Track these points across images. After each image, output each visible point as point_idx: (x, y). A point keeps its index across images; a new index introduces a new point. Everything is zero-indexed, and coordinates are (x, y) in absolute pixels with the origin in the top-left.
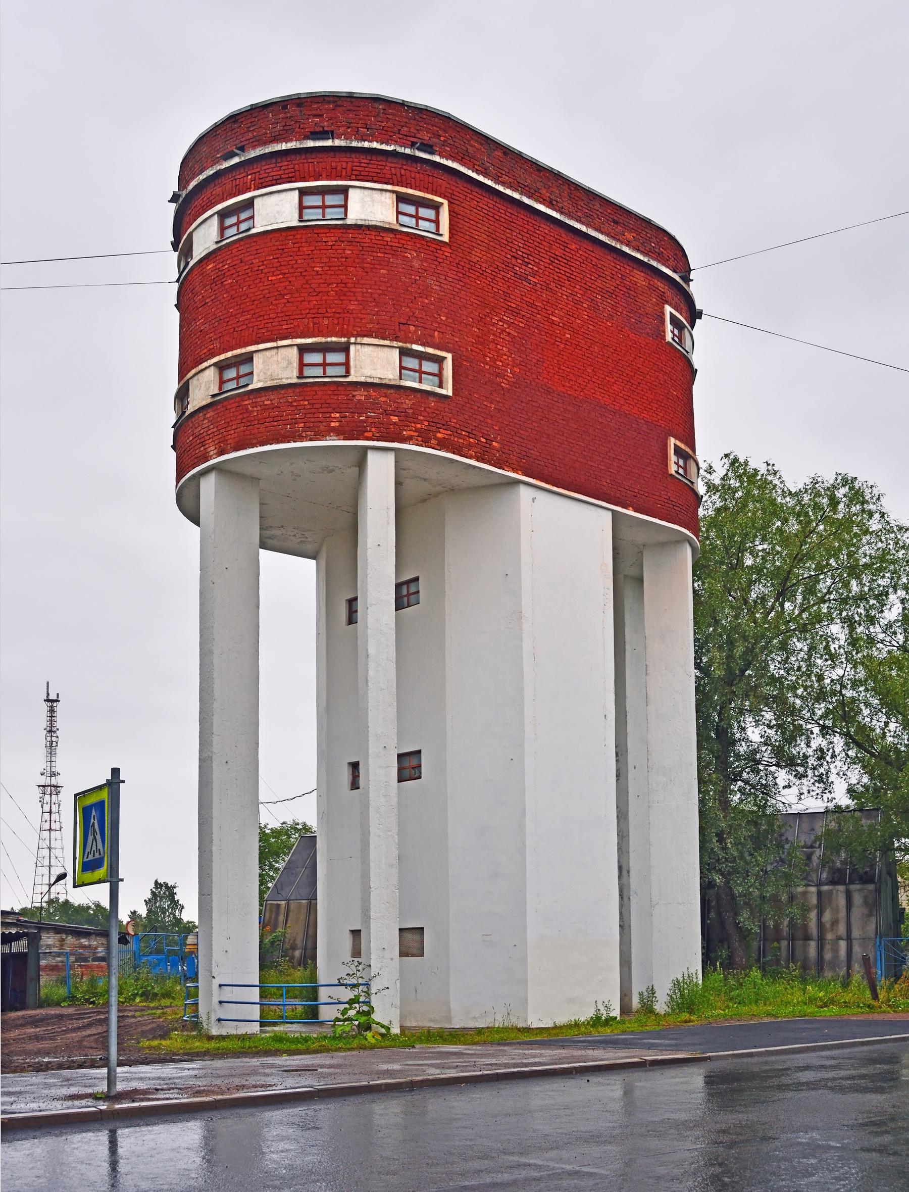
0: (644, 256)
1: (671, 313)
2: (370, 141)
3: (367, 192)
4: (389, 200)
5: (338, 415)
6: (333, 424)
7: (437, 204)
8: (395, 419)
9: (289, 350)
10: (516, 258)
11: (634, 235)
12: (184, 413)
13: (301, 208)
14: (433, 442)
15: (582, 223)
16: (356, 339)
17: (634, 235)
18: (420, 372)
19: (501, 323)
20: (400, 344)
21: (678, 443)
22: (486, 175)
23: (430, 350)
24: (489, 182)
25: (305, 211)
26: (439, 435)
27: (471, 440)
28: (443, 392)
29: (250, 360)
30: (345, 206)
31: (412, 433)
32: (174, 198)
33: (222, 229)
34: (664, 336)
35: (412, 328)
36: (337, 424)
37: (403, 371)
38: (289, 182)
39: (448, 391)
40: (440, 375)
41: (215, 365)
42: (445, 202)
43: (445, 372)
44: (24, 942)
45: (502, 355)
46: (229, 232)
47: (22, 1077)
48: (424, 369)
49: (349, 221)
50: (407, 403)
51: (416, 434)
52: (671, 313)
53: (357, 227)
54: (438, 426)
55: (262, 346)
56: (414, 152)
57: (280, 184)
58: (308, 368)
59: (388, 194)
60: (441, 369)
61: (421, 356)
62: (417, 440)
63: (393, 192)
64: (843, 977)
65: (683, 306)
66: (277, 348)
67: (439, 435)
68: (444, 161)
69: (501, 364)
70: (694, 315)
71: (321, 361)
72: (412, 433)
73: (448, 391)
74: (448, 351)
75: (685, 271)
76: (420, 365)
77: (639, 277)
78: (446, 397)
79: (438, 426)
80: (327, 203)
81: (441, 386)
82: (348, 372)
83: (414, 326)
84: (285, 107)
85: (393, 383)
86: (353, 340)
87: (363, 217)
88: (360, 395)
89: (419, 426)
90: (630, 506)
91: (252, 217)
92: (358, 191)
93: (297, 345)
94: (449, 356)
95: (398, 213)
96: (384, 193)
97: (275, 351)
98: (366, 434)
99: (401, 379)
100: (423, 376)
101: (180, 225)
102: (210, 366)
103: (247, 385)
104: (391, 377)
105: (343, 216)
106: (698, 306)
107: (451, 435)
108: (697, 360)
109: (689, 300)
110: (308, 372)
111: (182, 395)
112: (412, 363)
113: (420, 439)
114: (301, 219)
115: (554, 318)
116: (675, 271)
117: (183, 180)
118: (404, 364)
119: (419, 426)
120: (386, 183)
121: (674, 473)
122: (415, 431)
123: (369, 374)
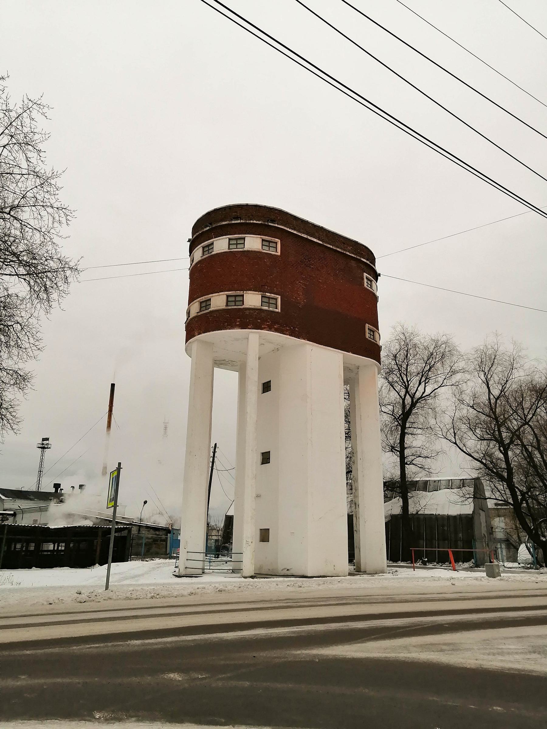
0: (355, 255)
1: (366, 276)
4: (260, 241)
5: (239, 320)
6: (237, 323)
8: (259, 321)
9: (223, 296)
10: (306, 259)
12: (189, 317)
13: (229, 244)
15: (330, 245)
18: (269, 303)
22: (295, 229)
24: (295, 232)
25: (229, 302)
26: (275, 327)
27: (288, 328)
28: (277, 310)
29: (210, 300)
30: (244, 243)
31: (265, 326)
32: (189, 240)
33: (203, 252)
34: (364, 285)
36: (239, 323)
37: (263, 246)
38: (225, 235)
39: (279, 310)
40: (276, 304)
41: (198, 301)
42: (279, 241)
43: (278, 303)
44: (126, 531)
45: (300, 295)
46: (206, 253)
48: (271, 302)
49: (245, 249)
50: (263, 315)
51: (267, 326)
52: (366, 276)
53: (248, 251)
54: (275, 323)
57: (222, 236)
58: (232, 245)
59: (259, 239)
60: (276, 302)
61: (269, 298)
63: (261, 238)
65: (372, 273)
66: (219, 295)
67: (275, 327)
68: (279, 226)
70: (376, 276)
71: (236, 243)
72: (265, 326)
73: (279, 310)
75: (372, 258)
76: (269, 301)
77: (353, 264)
78: (278, 312)
79: (275, 323)
80: (236, 300)
81: (276, 308)
82: (243, 304)
84: (225, 209)
86: (245, 292)
88: (247, 312)
89: (268, 323)
92: (248, 238)
94: (279, 297)
95: (262, 245)
97: (218, 296)
98: (249, 327)
99: (262, 306)
100: (270, 248)
101: (191, 251)
102: (195, 341)
103: (211, 253)
104: (258, 305)
105: (243, 247)
106: (378, 272)
107: (279, 326)
108: (378, 294)
109: (374, 271)
110: (231, 247)
111: (188, 313)
112: (265, 300)
113: (268, 328)
114: (229, 248)
116: (367, 260)
117: (193, 233)
118: (263, 300)
119: (268, 323)
120: (259, 235)
121: (368, 337)
123: (250, 304)
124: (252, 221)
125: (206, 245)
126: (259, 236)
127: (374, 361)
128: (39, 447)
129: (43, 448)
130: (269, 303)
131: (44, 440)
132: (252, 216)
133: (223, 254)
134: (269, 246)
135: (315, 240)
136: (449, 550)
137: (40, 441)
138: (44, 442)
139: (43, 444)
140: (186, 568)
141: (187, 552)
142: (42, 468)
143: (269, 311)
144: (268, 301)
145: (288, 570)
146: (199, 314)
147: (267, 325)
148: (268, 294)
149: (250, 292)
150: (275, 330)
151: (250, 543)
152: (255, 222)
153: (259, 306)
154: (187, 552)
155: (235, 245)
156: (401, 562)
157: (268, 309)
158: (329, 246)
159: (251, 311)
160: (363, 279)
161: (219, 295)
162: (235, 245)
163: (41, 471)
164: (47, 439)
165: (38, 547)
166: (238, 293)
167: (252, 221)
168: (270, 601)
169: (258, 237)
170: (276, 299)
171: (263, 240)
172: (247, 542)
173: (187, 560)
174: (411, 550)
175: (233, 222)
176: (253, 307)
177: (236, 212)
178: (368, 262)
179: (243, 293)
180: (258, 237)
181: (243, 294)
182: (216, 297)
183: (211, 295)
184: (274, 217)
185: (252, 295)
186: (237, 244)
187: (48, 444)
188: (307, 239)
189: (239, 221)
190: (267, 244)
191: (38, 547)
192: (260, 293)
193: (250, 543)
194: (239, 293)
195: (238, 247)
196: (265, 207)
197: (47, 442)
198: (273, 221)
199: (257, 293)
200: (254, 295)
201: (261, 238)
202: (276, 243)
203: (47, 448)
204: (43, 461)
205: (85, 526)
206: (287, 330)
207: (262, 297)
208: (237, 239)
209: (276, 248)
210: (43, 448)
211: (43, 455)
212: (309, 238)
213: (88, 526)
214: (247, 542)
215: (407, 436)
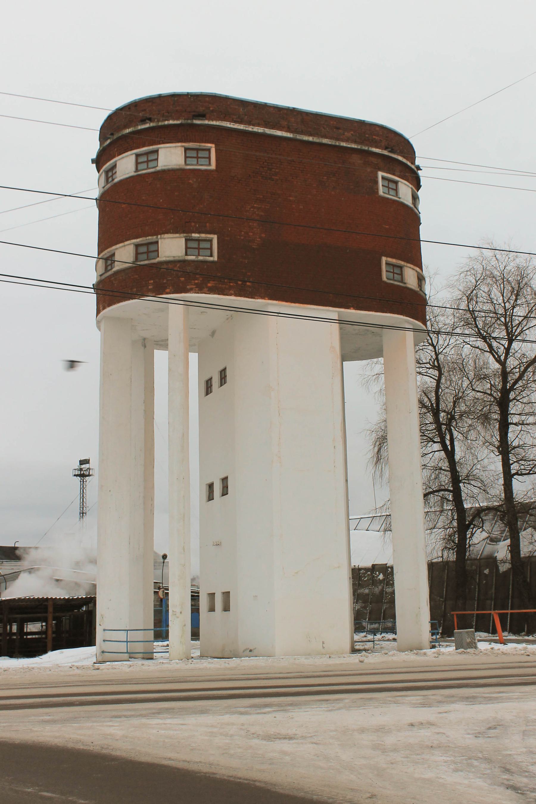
2: (168, 120)
3: (168, 149)
5: (152, 281)
7: (209, 148)
8: (183, 279)
11: (352, 133)
14: (206, 290)
16: (161, 236)
17: (352, 133)
19: (252, 209)
20: (185, 235)
21: (390, 260)
22: (241, 122)
23: (203, 235)
24: (241, 127)
34: (378, 192)
35: (193, 224)
39: (215, 258)
40: (211, 249)
42: (212, 147)
47: (184, 679)
48: (201, 246)
50: (189, 269)
51: (195, 287)
53: (164, 172)
55: (118, 246)
56: (193, 122)
59: (180, 148)
61: (198, 240)
62: (195, 290)
63: (182, 146)
64: (381, 634)
69: (252, 234)
74: (214, 234)
77: (356, 159)
82: (158, 257)
83: (194, 222)
84: (129, 108)
85: (181, 258)
86: (159, 236)
87: (166, 164)
89: (196, 281)
90: (351, 307)
91: (157, 159)
93: (133, 243)
94: (215, 238)
95: (186, 157)
96: (177, 148)
97: (123, 248)
99: (186, 254)
104: (180, 255)
112: (194, 245)
113: (197, 289)
115: (291, 198)
119: (196, 281)
122: (194, 285)
124: (166, 123)
125: (109, 168)
126: (179, 144)
127: (401, 317)
128: (75, 475)
129: (82, 475)
130: (199, 249)
131: (82, 462)
132: (168, 113)
133: (128, 180)
134: (197, 158)
135: (279, 133)
136: (492, 612)
137: (77, 465)
138: (83, 466)
139: (81, 470)
140: (103, 652)
141: (104, 630)
142: (84, 508)
143: (197, 261)
144: (387, 185)
145: (251, 651)
146: (103, 277)
147: (195, 284)
148: (195, 235)
149: (166, 236)
150: (208, 291)
151: (178, 614)
152: (171, 122)
153: (182, 256)
154: (104, 630)
155: (146, 164)
156: (509, 633)
157: (196, 259)
158: (306, 138)
159: (170, 266)
160: (376, 182)
161: (125, 246)
162: (146, 164)
163: (83, 513)
164: (86, 462)
165: (21, 628)
166: (149, 239)
167: (166, 123)
168: (16, 687)
169: (178, 146)
170: (211, 241)
171: (186, 149)
172: (175, 613)
173: (104, 641)
174: (453, 615)
175: (140, 127)
176: (171, 259)
177: (145, 110)
178: (386, 153)
179: (157, 238)
180: (178, 146)
181: (156, 240)
182: (121, 250)
183: (114, 247)
184: (203, 109)
185: (169, 240)
186: (148, 161)
187: (89, 469)
188: (263, 135)
189: (147, 126)
190: (194, 154)
191: (21, 628)
192: (182, 235)
193: (178, 614)
194: (150, 239)
195: (149, 166)
196: (188, 96)
197: (87, 466)
198: (202, 116)
199: (177, 235)
200: (174, 239)
201: (182, 146)
202: (209, 150)
203: (89, 475)
204: (85, 496)
205: (27, 598)
206: (230, 288)
207: (187, 240)
208: (147, 154)
209: (209, 158)
210: (82, 475)
211: (83, 486)
212: (268, 131)
213: (32, 597)
214: (175, 613)
215: (511, 428)
